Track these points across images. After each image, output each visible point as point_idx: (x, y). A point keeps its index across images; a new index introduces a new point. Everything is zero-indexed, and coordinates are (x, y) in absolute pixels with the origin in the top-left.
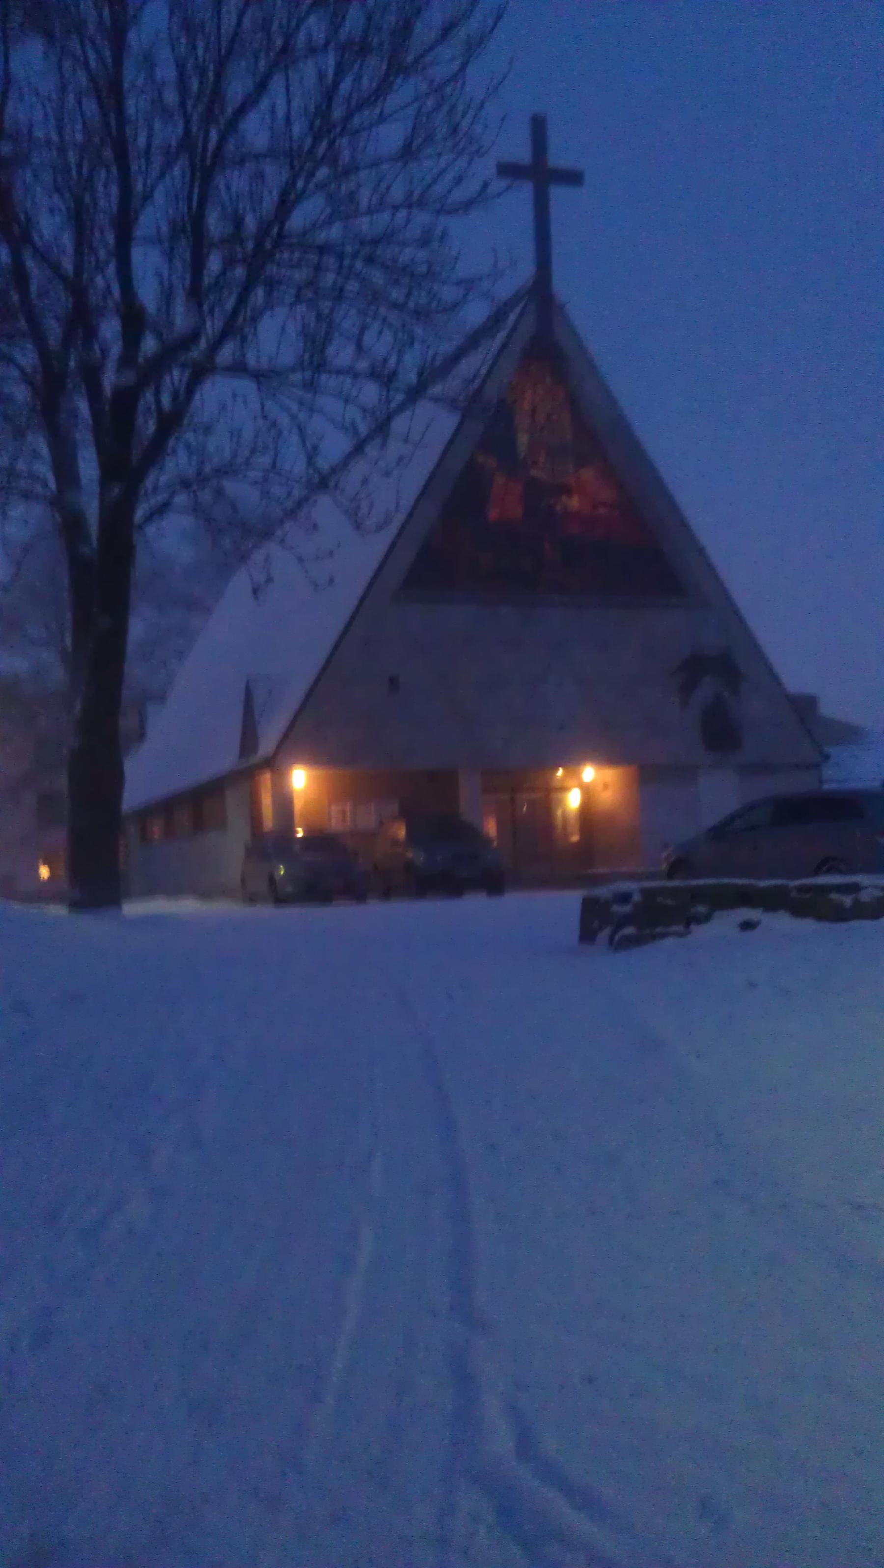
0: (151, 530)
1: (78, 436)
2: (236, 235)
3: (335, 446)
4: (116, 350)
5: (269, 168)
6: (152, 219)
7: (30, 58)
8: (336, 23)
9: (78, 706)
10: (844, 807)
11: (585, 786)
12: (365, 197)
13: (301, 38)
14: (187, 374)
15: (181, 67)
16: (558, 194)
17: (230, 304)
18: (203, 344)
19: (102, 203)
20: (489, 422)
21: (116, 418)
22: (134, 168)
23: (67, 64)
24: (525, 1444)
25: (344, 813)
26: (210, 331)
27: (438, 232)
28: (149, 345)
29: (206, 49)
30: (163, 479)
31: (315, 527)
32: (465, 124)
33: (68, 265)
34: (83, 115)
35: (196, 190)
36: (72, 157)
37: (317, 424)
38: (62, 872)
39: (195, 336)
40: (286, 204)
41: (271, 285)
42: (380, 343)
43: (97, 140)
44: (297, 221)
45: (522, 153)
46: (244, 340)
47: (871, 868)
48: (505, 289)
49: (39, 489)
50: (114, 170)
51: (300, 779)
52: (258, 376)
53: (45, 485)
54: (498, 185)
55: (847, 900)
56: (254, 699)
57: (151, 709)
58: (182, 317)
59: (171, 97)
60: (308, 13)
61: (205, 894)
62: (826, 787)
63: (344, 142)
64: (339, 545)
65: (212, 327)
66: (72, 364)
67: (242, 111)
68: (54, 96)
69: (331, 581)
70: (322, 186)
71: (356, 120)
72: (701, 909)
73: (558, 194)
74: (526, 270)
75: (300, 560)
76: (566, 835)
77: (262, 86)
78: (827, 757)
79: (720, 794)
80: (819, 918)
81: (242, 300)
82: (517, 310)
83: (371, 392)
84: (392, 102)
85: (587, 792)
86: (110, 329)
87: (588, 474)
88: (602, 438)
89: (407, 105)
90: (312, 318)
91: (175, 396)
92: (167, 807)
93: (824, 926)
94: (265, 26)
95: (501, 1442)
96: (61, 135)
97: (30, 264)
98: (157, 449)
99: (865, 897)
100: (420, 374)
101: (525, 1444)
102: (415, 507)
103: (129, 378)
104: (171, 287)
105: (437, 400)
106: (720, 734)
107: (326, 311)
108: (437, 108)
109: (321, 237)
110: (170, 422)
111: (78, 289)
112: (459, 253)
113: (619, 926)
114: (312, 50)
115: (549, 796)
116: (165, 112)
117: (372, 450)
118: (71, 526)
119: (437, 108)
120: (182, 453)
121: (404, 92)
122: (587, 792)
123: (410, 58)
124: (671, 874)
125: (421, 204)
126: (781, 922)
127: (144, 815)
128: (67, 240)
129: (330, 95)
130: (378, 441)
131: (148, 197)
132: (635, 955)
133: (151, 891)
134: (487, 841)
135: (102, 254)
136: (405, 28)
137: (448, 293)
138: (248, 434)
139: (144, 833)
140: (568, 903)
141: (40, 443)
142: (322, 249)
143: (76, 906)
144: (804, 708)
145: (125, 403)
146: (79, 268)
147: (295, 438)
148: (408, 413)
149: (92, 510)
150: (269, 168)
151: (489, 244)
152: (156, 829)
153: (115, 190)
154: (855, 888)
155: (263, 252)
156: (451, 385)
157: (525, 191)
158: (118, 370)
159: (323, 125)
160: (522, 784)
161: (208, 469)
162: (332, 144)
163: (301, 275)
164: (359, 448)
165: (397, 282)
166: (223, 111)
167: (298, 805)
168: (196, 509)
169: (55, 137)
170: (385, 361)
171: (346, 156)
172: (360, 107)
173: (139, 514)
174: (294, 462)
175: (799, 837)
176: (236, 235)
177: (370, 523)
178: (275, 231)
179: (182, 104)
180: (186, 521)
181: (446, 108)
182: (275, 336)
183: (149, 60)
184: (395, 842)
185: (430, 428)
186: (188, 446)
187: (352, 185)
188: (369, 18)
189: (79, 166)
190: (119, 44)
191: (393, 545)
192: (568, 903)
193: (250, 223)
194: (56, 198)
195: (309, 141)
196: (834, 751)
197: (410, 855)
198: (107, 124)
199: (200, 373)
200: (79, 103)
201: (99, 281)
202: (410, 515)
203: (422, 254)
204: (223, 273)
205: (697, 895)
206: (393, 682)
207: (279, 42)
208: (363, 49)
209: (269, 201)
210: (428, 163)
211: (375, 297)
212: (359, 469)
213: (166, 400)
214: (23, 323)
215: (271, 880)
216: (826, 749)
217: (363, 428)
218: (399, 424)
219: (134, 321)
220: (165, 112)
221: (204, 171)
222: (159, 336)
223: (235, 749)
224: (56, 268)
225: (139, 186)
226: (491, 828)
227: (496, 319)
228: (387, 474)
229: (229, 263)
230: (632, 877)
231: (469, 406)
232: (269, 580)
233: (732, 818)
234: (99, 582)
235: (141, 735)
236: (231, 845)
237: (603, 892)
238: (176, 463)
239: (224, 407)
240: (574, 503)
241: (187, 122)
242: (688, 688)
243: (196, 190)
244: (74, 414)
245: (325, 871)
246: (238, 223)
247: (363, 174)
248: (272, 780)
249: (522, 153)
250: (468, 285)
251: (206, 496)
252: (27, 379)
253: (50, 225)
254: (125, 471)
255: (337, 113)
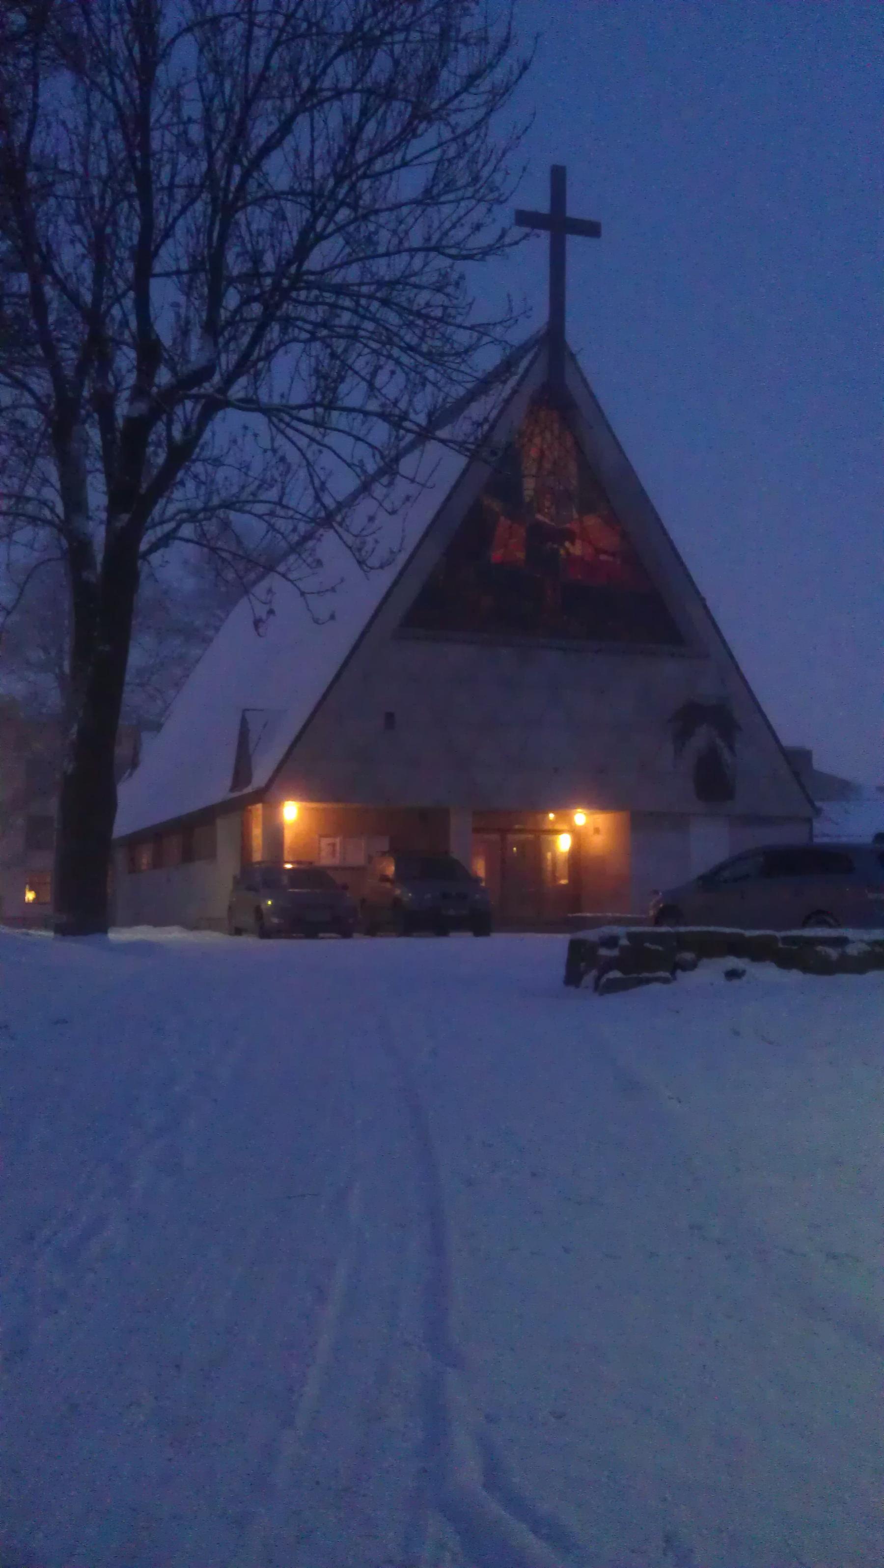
0: (155, 558)
1: (88, 464)
2: (255, 275)
3: (344, 483)
4: (131, 380)
5: (289, 208)
6: (172, 254)
7: (59, 90)
8: (364, 68)
9: (75, 729)
10: (833, 861)
11: (577, 830)
12: (384, 236)
13: (327, 82)
14: (199, 408)
15: (207, 100)
16: (574, 243)
17: (245, 340)
18: (217, 378)
19: (123, 234)
20: (496, 466)
21: (126, 450)
22: (156, 204)
23: (97, 97)
24: (493, 1475)
25: (334, 845)
26: (224, 367)
27: (454, 276)
28: (164, 377)
29: (233, 87)
30: (171, 509)
31: (319, 563)
32: (485, 173)
33: (88, 298)
34: (108, 144)
35: (217, 227)
36: (95, 190)
37: (327, 460)
38: (48, 898)
39: (204, 373)
40: (302, 250)
41: (287, 322)
42: (392, 385)
43: (121, 172)
44: (315, 261)
45: (542, 204)
46: (257, 374)
47: (865, 921)
48: (519, 334)
49: (47, 513)
50: (137, 204)
51: (292, 812)
52: (267, 411)
53: (52, 510)
54: (517, 232)
55: (833, 953)
56: (251, 726)
57: (145, 736)
58: (197, 350)
59: (196, 133)
60: (336, 56)
61: (192, 926)
62: (817, 840)
63: (366, 184)
64: (342, 580)
65: (228, 361)
66: (85, 394)
67: (265, 151)
68: (81, 129)
69: (332, 617)
70: (340, 229)
71: (378, 166)
72: (688, 956)
73: (574, 243)
74: (540, 319)
75: (303, 594)
76: (555, 878)
77: (286, 128)
78: (818, 811)
79: (709, 844)
80: (806, 969)
81: (256, 339)
82: (530, 356)
83: (380, 432)
84: (415, 147)
85: (578, 836)
86: (125, 359)
87: (591, 521)
88: (608, 488)
89: (432, 149)
90: (324, 355)
91: (186, 430)
92: (156, 835)
93: (809, 977)
94: (292, 69)
95: (469, 1472)
96: (85, 165)
97: (50, 292)
98: (165, 481)
99: (852, 950)
100: (430, 415)
101: (493, 1475)
102: (418, 547)
103: (142, 407)
104: (188, 322)
105: (443, 441)
106: (713, 783)
107: (340, 350)
108: (459, 156)
109: (337, 278)
110: (181, 454)
111: (95, 318)
112: (474, 300)
113: (604, 970)
114: (338, 94)
115: (540, 838)
116: (190, 148)
117: (378, 490)
118: (77, 551)
119: (459, 156)
120: (190, 485)
121: (430, 135)
122: (578, 836)
123: (435, 105)
124: (658, 921)
125: (438, 249)
126: (767, 973)
127: (134, 841)
128: (86, 269)
129: (353, 139)
130: (385, 480)
131: (168, 233)
132: (614, 1000)
133: (135, 921)
134: (477, 880)
135: (121, 285)
136: (431, 77)
137: (463, 338)
138: (256, 470)
139: (133, 866)
140: (556, 945)
141: (49, 468)
142: (340, 290)
143: (63, 930)
144: (798, 761)
145: (138, 429)
146: (97, 299)
147: (303, 473)
148: (417, 453)
149: (98, 534)
150: (289, 208)
151: (503, 291)
152: (145, 859)
153: (137, 223)
154: (842, 942)
155: (280, 291)
156: (460, 429)
157: (543, 240)
158: (131, 400)
159: (345, 169)
160: (512, 824)
161: (216, 501)
162: (352, 188)
163: (316, 314)
164: (365, 488)
165: (410, 325)
166: (247, 147)
167: (289, 837)
168: (201, 540)
169: (80, 169)
170: (395, 403)
171: (367, 198)
172: (382, 152)
173: (143, 546)
174: (301, 499)
175: (785, 889)
176: (255, 275)
177: (374, 561)
178: (293, 269)
179: (208, 142)
180: (190, 551)
181: (467, 156)
182: (288, 374)
183: (176, 97)
184: (385, 879)
185: (439, 467)
186: (196, 477)
187: (372, 227)
188: (396, 63)
189: (102, 199)
190: (148, 83)
191: (395, 583)
192: (556, 945)
193: (269, 262)
194: (78, 229)
195: (331, 182)
196: (829, 808)
197: (398, 892)
198: (132, 158)
199: (213, 406)
200: (105, 137)
201: (116, 311)
202: (412, 557)
203: (440, 298)
204: (238, 310)
205: (683, 943)
206: (390, 718)
207: (305, 84)
208: (388, 95)
209: (289, 240)
210: (446, 210)
211: (390, 338)
212: (366, 506)
213: (177, 433)
214: (39, 351)
215: (258, 912)
216: (818, 804)
217: (371, 467)
218: (407, 465)
219: (150, 352)
220: (190, 148)
221: (226, 209)
222: (173, 370)
223: (228, 782)
224: (74, 298)
225: (161, 220)
226: (480, 868)
227: (507, 367)
228: (393, 512)
229: (247, 300)
230: (618, 921)
231: (476, 450)
232: (271, 612)
233: (721, 868)
234: (101, 608)
235: (134, 763)
236: (219, 877)
237: (591, 935)
238: (184, 495)
239: (235, 442)
240: (577, 549)
241: (211, 155)
242: (682, 736)
243: (217, 227)
244: (86, 441)
245: (312, 905)
246: (257, 259)
247: (383, 218)
248: (264, 808)
249: (542, 204)
250: (482, 329)
251: (212, 527)
252: (41, 406)
253: (71, 256)
254: (133, 499)
255: (360, 157)
